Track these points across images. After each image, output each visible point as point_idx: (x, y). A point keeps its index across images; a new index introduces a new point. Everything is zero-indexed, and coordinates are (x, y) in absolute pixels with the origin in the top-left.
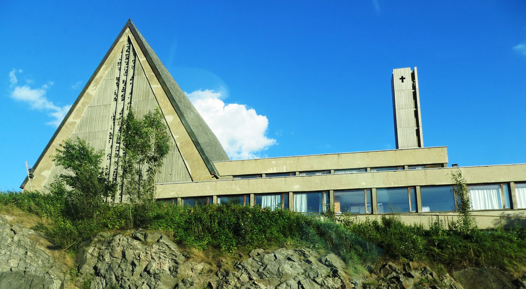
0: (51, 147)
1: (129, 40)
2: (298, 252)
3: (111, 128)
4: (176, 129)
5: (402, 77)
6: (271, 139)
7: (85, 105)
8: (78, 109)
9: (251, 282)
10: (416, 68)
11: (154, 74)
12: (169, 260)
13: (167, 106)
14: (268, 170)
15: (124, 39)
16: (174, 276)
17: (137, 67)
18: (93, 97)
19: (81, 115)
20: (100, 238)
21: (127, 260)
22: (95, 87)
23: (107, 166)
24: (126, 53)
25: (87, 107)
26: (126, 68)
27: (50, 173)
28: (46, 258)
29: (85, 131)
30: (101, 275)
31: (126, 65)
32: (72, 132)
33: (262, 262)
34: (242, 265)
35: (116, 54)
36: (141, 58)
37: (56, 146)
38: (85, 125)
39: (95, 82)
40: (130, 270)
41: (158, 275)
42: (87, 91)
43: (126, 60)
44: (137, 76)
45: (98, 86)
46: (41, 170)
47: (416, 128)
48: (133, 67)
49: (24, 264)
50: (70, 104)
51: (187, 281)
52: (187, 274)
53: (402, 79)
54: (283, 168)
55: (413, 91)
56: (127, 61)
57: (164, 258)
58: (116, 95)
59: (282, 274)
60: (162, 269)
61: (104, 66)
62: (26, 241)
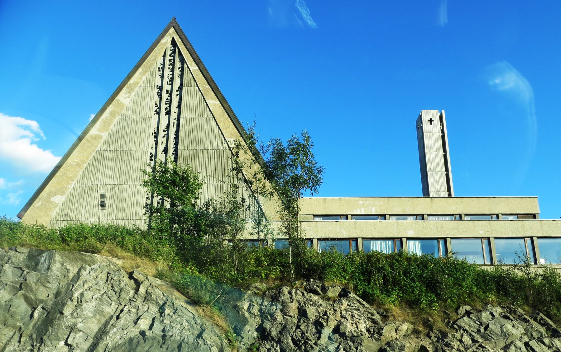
1: (174, 42)
2: (506, 310)
3: (152, 148)
5: (431, 119)
7: (115, 116)
9: (477, 345)
10: (443, 112)
11: (210, 87)
12: (365, 319)
13: (229, 127)
14: (355, 211)
15: (166, 41)
16: (377, 340)
18: (126, 106)
19: (109, 128)
20: (255, 290)
21: (308, 320)
22: (128, 94)
26: (171, 76)
27: (64, 199)
28: (191, 317)
29: (115, 148)
30: (273, 339)
31: (170, 71)
32: (96, 147)
33: (480, 321)
34: (458, 325)
35: (157, 57)
36: (192, 66)
37: (72, 164)
38: (114, 140)
40: (314, 332)
41: (359, 338)
42: (117, 98)
43: (169, 65)
44: (187, 87)
45: (133, 94)
47: (446, 173)
49: (160, 326)
50: (94, 114)
51: (395, 345)
52: (391, 336)
53: (431, 121)
54: (371, 209)
55: (442, 134)
56: (171, 67)
57: (358, 317)
58: (157, 107)
59: (509, 334)
60: (360, 330)
61: (140, 70)
62: (157, 293)
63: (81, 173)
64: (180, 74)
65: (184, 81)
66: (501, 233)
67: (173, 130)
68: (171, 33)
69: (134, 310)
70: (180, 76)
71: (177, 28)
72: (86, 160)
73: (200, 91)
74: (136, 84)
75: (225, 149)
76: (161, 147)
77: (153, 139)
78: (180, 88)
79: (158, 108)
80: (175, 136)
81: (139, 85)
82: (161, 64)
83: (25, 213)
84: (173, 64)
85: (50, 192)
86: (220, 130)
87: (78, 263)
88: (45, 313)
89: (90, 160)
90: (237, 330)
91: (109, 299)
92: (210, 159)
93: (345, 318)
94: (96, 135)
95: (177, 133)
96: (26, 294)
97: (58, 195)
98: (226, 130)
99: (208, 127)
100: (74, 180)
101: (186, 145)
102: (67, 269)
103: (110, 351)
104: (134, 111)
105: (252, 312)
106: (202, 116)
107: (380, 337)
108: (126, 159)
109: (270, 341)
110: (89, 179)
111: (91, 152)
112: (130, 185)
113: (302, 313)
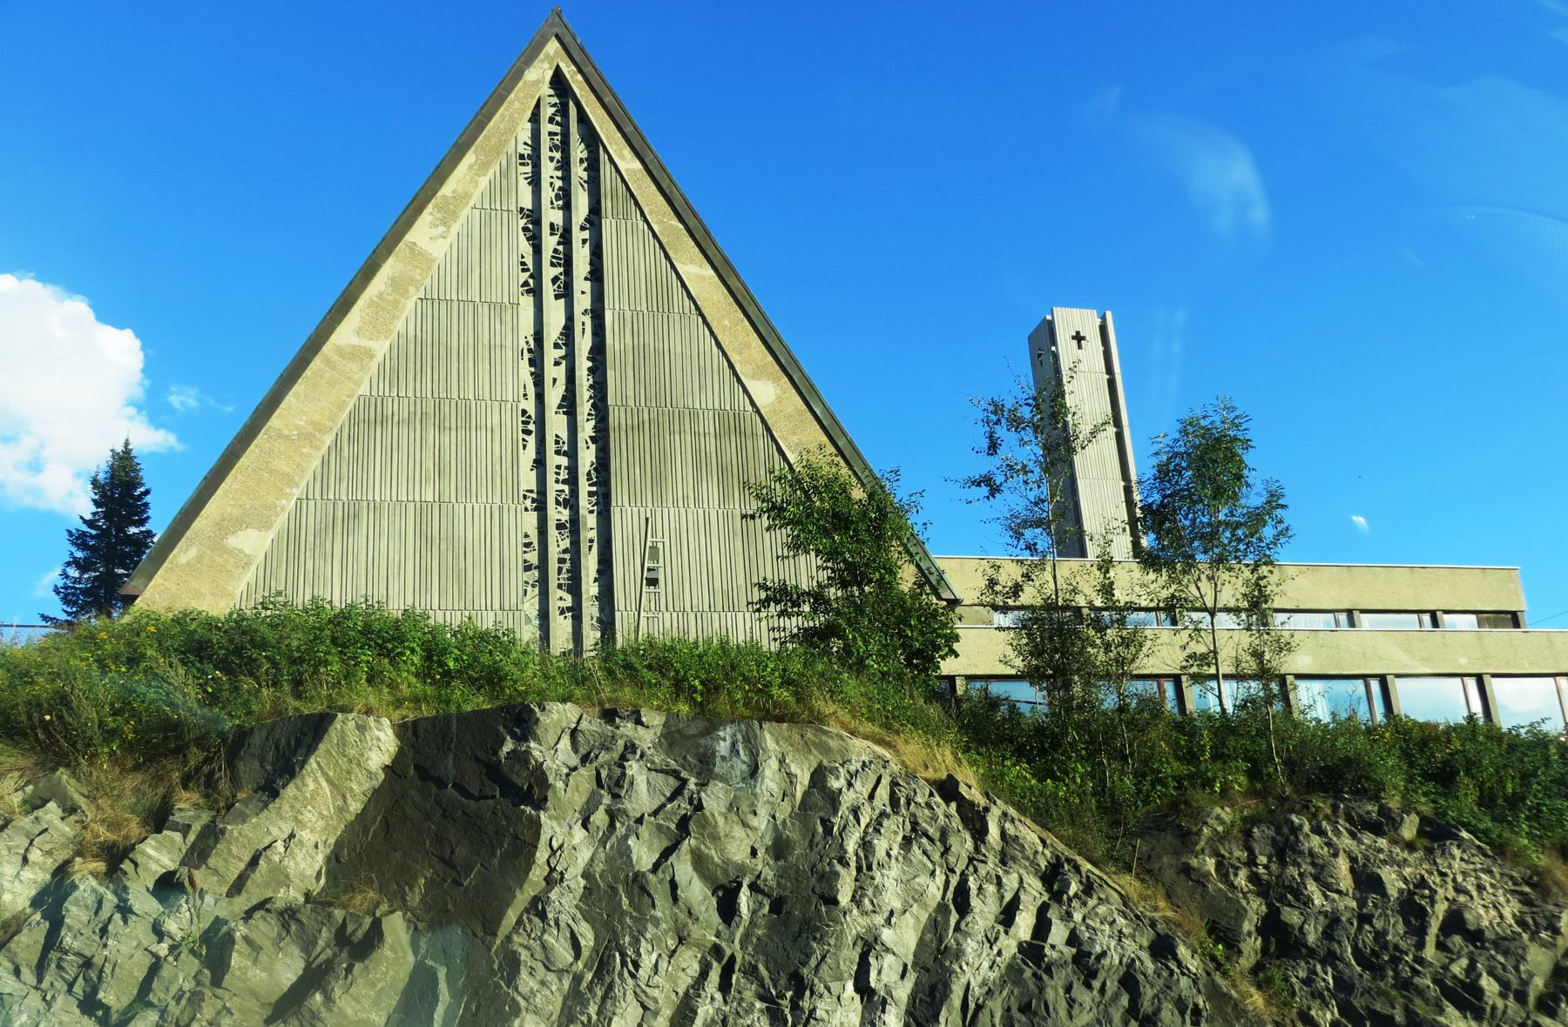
0: (261, 438)
1: (559, 82)
4: (794, 433)
6: (157, 428)
8: (375, 299)
10: (1109, 315)
11: (681, 226)
15: (538, 75)
17: (609, 188)
19: (392, 327)
22: (441, 229)
23: (526, 536)
24: (550, 125)
25: (414, 299)
26: (559, 183)
30: (1311, 953)
32: (358, 384)
36: (622, 157)
37: (286, 432)
39: (435, 206)
40: (1401, 932)
41: (1517, 944)
45: (456, 228)
46: (229, 525)
48: (585, 182)
53: (1079, 338)
58: (529, 273)
61: (470, 158)
63: (317, 462)
64: (586, 178)
65: (603, 200)
66: (1507, 663)
67: (584, 343)
68: (552, 53)
69: (991, 889)
70: (586, 185)
71: (567, 39)
72: (331, 424)
73: (655, 236)
74: (462, 198)
75: (742, 409)
76: (554, 395)
77: (526, 371)
78: (594, 219)
79: (531, 276)
80: (590, 364)
81: (471, 204)
82: (525, 144)
83: (146, 586)
84: (565, 147)
85: (223, 519)
86: (724, 354)
87: (812, 757)
88: (765, 902)
89: (341, 422)
91: (925, 859)
92: (623, 433)
93: (1466, 892)
94: (353, 346)
95: (598, 351)
96: (700, 849)
97: (249, 530)
98: (740, 353)
99: (684, 339)
100: (297, 486)
101: (630, 393)
102: (789, 774)
104: (462, 281)
105: (1236, 883)
106: (666, 310)
107: (1554, 939)
108: (453, 426)
109: (1304, 958)
110: (344, 484)
111: (344, 398)
112: (475, 504)
113: (1367, 882)
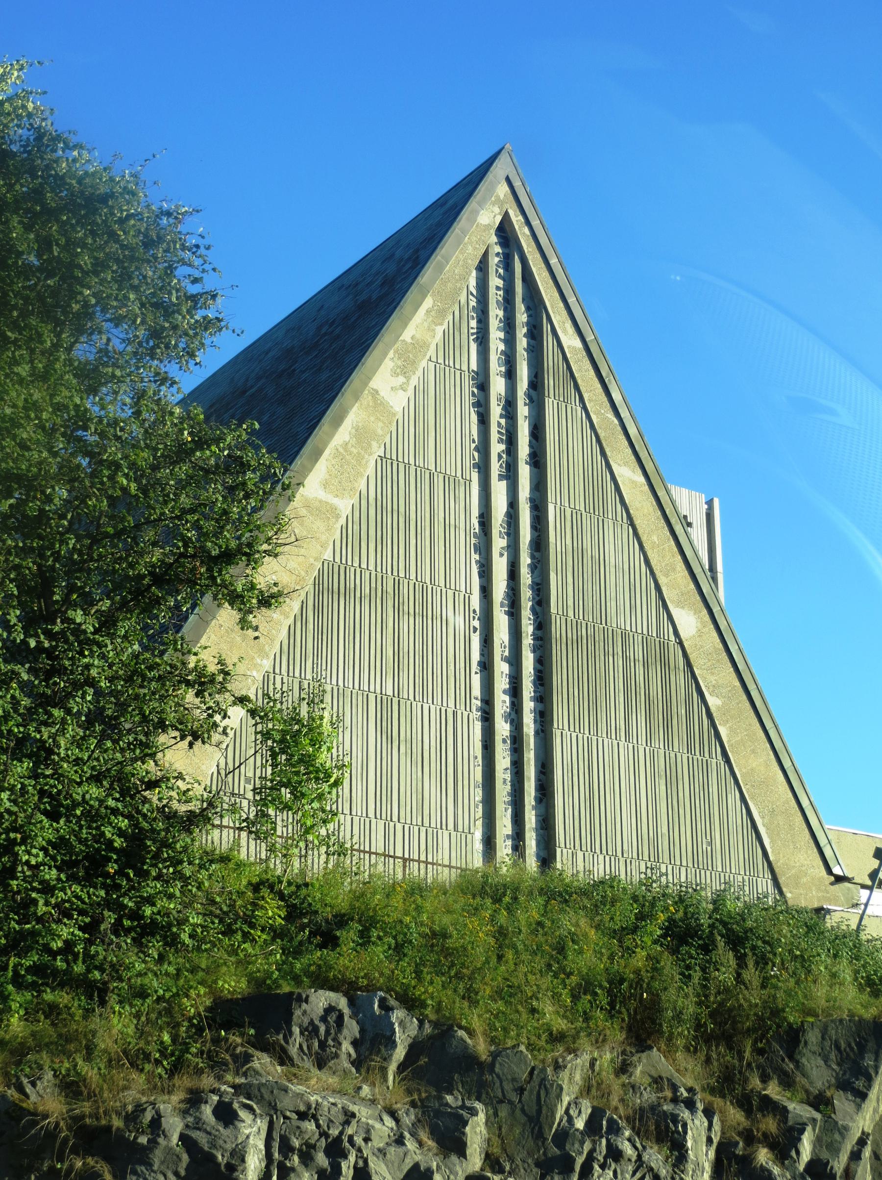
1: (505, 232)
22: (401, 379)
36: (565, 331)
90: (67, 905)
98: (667, 575)
103: (283, 1132)
